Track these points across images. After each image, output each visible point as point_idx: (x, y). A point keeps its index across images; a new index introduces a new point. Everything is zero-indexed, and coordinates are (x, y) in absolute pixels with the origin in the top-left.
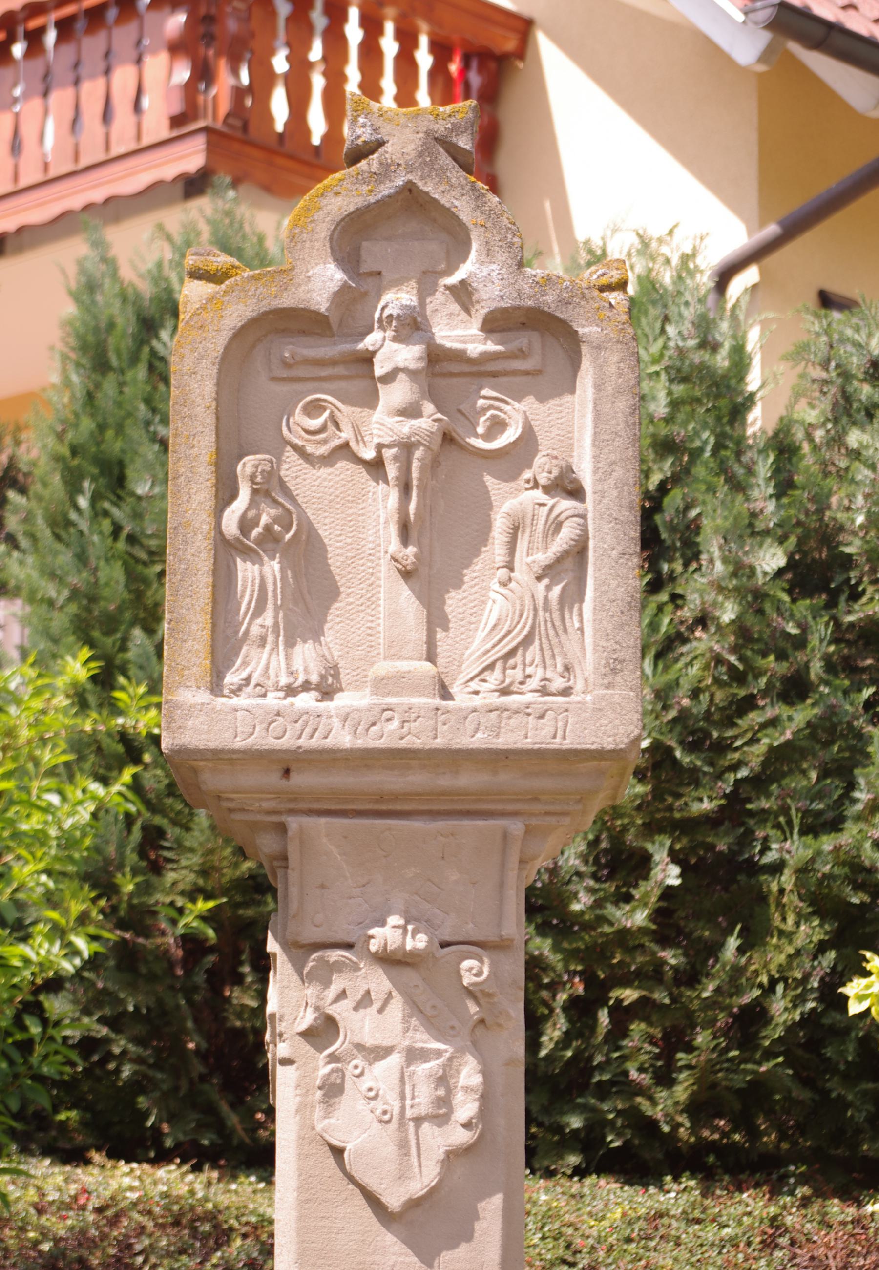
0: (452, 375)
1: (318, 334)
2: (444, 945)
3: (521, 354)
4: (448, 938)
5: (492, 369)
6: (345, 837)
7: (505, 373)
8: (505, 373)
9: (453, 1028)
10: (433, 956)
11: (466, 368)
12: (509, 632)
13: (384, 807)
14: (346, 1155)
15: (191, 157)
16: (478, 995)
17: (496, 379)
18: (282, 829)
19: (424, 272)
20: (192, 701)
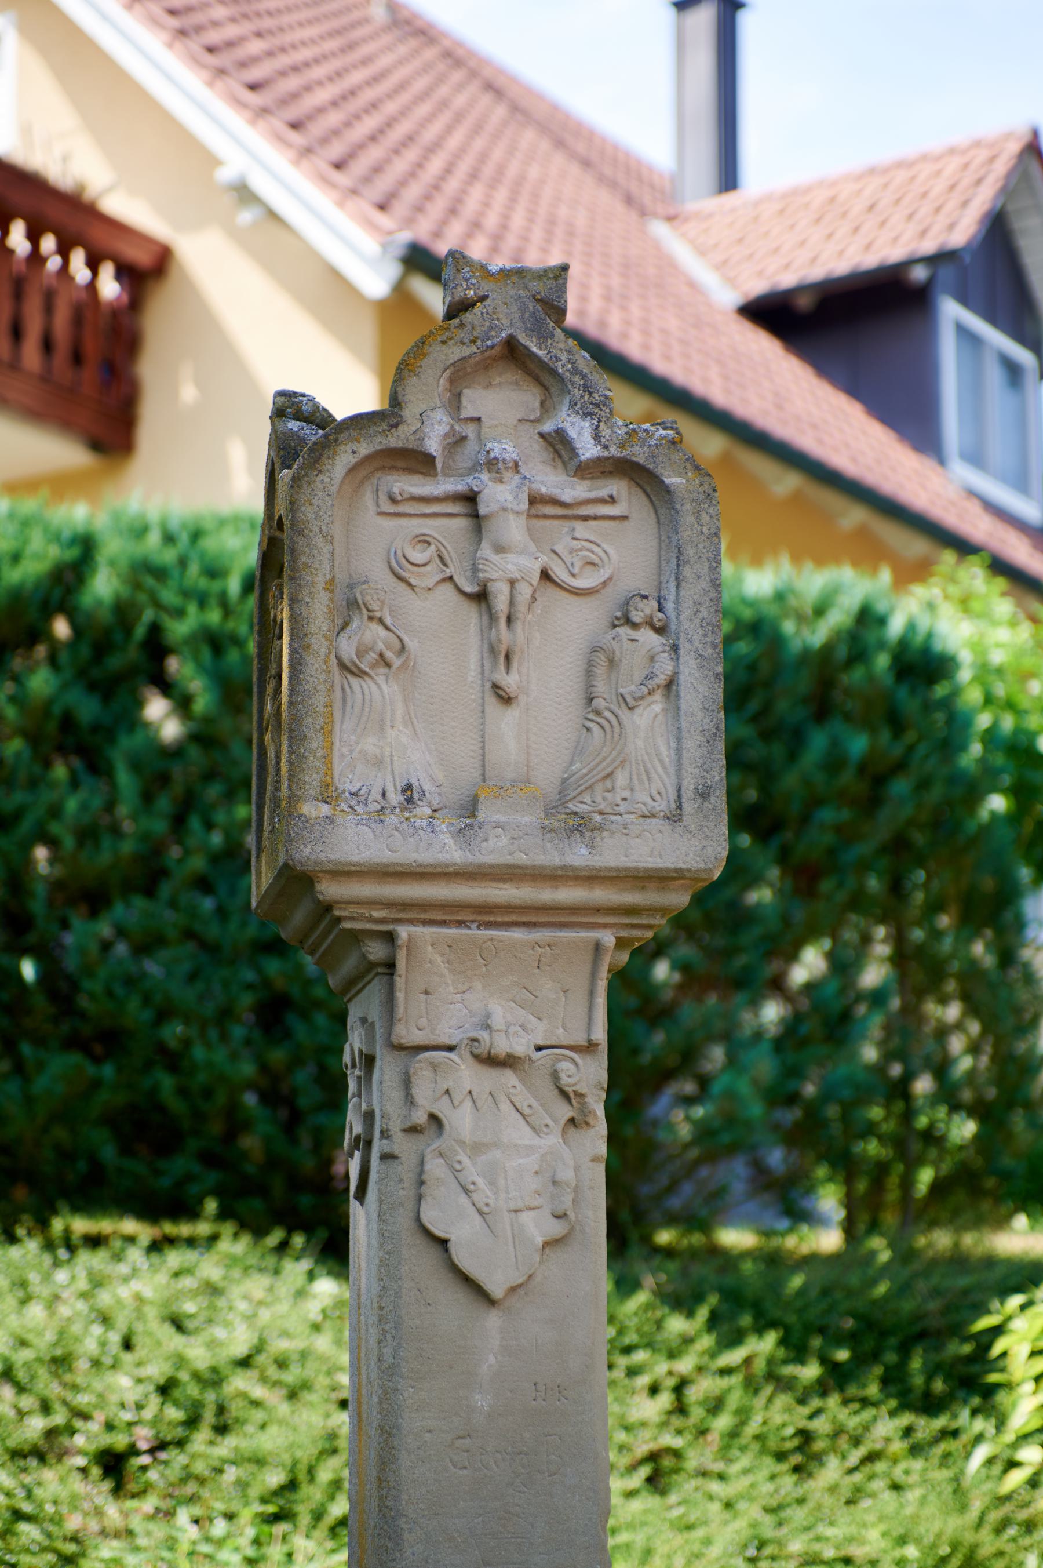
0: (546, 517)
1: (422, 473)
2: (539, 1048)
3: (612, 500)
4: (541, 1043)
5: (584, 513)
6: (450, 946)
7: (595, 518)
8: (595, 518)
9: (547, 1126)
10: (530, 1059)
11: (560, 511)
12: (605, 758)
13: (489, 915)
14: (450, 1245)
16: (572, 1095)
17: (586, 523)
18: (390, 937)
19: (520, 420)
20: (314, 814)
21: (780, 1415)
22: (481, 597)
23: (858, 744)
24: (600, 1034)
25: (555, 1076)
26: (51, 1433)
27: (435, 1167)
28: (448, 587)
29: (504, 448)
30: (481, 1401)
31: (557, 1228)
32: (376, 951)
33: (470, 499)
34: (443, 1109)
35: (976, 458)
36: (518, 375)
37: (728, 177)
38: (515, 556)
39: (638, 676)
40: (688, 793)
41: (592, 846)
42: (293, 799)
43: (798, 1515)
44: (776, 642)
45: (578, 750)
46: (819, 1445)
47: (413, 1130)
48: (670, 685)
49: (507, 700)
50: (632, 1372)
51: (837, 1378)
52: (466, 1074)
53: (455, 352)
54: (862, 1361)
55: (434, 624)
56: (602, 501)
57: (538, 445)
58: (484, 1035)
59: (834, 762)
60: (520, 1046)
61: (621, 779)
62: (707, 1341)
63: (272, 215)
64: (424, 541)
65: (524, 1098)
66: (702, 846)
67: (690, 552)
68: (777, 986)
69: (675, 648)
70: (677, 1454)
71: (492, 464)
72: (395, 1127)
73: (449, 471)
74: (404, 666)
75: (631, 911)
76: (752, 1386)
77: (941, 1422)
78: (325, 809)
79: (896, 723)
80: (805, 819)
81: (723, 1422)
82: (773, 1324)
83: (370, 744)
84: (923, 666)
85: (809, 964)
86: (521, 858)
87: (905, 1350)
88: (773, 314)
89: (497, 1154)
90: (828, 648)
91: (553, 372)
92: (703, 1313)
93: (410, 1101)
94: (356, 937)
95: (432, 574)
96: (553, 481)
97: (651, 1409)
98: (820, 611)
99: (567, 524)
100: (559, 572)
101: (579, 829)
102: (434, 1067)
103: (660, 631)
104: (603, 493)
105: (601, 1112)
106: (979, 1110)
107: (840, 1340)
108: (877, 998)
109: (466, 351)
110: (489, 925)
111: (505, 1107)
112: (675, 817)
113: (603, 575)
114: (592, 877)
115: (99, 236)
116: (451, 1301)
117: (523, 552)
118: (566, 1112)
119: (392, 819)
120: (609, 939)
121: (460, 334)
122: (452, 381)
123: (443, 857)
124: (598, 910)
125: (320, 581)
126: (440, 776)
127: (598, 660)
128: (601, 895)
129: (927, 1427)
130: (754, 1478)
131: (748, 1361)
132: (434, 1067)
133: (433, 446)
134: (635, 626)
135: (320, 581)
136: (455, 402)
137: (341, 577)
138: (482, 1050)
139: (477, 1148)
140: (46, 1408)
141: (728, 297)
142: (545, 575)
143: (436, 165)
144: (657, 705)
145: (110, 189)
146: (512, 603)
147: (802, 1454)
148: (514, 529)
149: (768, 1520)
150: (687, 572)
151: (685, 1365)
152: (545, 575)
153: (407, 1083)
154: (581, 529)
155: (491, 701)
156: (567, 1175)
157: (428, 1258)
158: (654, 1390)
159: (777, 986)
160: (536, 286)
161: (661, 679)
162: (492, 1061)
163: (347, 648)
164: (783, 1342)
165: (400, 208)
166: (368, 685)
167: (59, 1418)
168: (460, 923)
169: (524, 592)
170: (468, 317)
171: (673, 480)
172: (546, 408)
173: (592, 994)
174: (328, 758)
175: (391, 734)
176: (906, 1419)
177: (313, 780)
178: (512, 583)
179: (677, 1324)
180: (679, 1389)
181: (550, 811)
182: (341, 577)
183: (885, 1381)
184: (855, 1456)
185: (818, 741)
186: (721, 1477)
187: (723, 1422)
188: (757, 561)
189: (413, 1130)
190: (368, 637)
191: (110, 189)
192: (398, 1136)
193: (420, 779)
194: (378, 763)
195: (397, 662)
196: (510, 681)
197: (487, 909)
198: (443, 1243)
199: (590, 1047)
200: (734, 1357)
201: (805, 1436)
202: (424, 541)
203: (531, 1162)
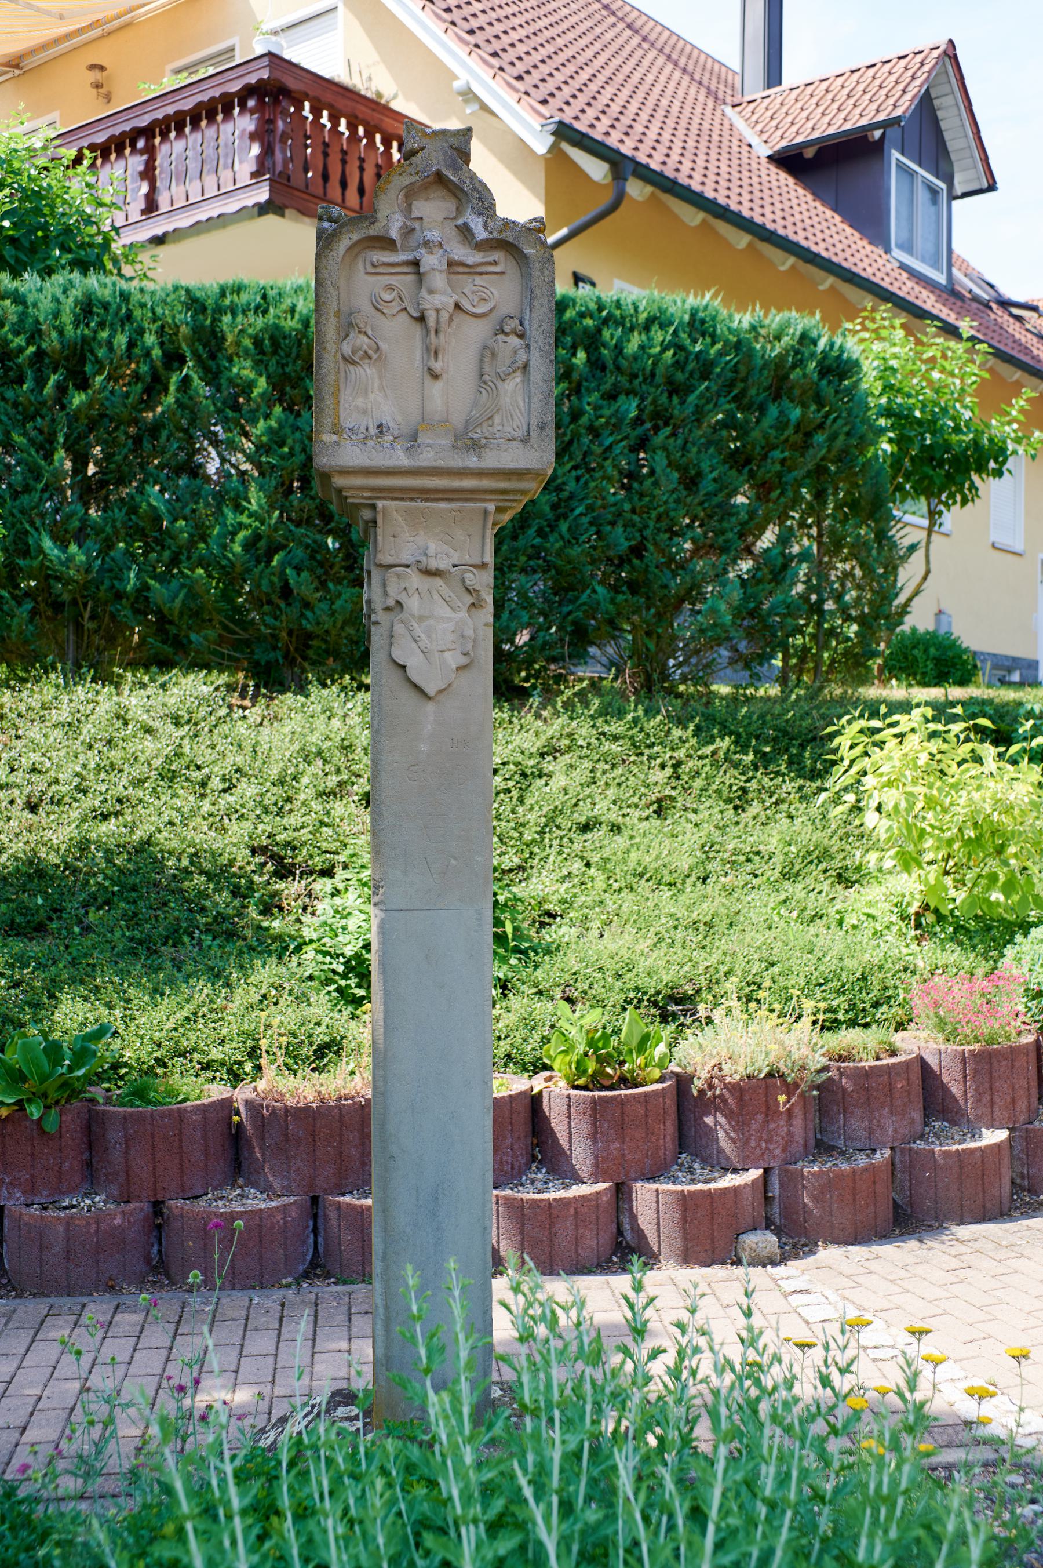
3: (495, 263)
15: (262, 194)
18: (373, 507)
21: (731, 778)
22: (422, 319)
23: (796, 413)
24: (489, 558)
25: (463, 581)
26: (340, 784)
27: (399, 628)
28: (404, 315)
29: (434, 234)
30: (424, 748)
31: (464, 660)
32: (367, 514)
33: (416, 263)
34: (403, 598)
35: (908, 247)
36: (445, 193)
37: (773, 75)
38: (440, 297)
39: (508, 362)
40: (533, 427)
41: (480, 456)
43: (734, 831)
44: (750, 353)
45: (475, 404)
46: (750, 796)
47: (388, 609)
48: (526, 366)
49: (436, 377)
50: (650, 758)
51: (764, 760)
52: (415, 580)
53: (407, 180)
54: (777, 752)
55: (396, 334)
56: (490, 264)
57: (454, 232)
58: (424, 559)
59: (782, 424)
60: (443, 564)
61: (497, 419)
62: (693, 741)
63: (485, 108)
64: (390, 288)
65: (446, 592)
66: (541, 457)
67: (537, 291)
68: (749, 551)
69: (528, 346)
70: (673, 799)
71: (426, 244)
73: (405, 249)
74: (379, 358)
75: (504, 492)
76: (716, 765)
78: (335, 437)
79: (819, 400)
80: (765, 457)
81: (698, 783)
82: (730, 734)
83: (360, 402)
84: (839, 369)
85: (768, 539)
86: (441, 463)
87: (802, 747)
88: (790, 161)
89: (432, 622)
90: (782, 357)
91: (462, 190)
92: (692, 727)
93: (386, 594)
94: (357, 506)
95: (395, 307)
96: (462, 253)
97: (660, 776)
98: (778, 338)
99: (469, 278)
100: (465, 304)
101: (472, 447)
102: (398, 576)
103: (521, 336)
104: (490, 259)
105: (490, 600)
106: (861, 620)
108: (804, 556)
109: (413, 179)
110: (427, 500)
111: (436, 597)
112: (526, 440)
114: (481, 473)
115: (389, 124)
116: (408, 697)
117: (444, 293)
118: (469, 600)
119: (370, 443)
120: (491, 507)
121: (410, 170)
122: (407, 197)
123: (398, 463)
124: (486, 491)
125: (332, 311)
126: (399, 419)
127: (487, 353)
128: (486, 483)
130: (712, 811)
131: (714, 753)
132: (398, 576)
133: (394, 234)
134: (506, 334)
135: (332, 311)
136: (408, 209)
137: (344, 309)
138: (423, 566)
139: (421, 619)
140: (338, 771)
141: (765, 151)
142: (457, 306)
143: (584, 76)
144: (518, 378)
145: (395, 97)
146: (438, 322)
147: (740, 801)
148: (439, 280)
149: (717, 833)
150: (536, 303)
151: (681, 754)
152: (457, 306)
153: (384, 585)
154: (478, 280)
155: (427, 377)
156: (469, 632)
157: (396, 675)
158: (663, 766)
159: (749, 551)
160: (452, 141)
161: (520, 364)
163: (347, 348)
164: (736, 743)
165: (556, 103)
166: (358, 369)
167: (345, 777)
168: (412, 499)
169: (445, 316)
170: (414, 159)
171: (528, 251)
172: (459, 211)
173: (484, 537)
174: (336, 410)
175: (372, 396)
177: (328, 421)
178: (438, 311)
179: (677, 732)
180: (678, 765)
181: (457, 438)
182: (344, 309)
183: (790, 763)
184: (769, 802)
185: (773, 411)
186: (695, 811)
187: (698, 783)
188: (742, 308)
189: (388, 609)
190: (358, 342)
191: (395, 97)
192: (380, 613)
193: (387, 420)
194: (365, 412)
195: (375, 356)
196: (437, 366)
197: (425, 491)
199: (483, 566)
200: (708, 750)
201: (744, 791)
202: (390, 288)
203: (450, 626)
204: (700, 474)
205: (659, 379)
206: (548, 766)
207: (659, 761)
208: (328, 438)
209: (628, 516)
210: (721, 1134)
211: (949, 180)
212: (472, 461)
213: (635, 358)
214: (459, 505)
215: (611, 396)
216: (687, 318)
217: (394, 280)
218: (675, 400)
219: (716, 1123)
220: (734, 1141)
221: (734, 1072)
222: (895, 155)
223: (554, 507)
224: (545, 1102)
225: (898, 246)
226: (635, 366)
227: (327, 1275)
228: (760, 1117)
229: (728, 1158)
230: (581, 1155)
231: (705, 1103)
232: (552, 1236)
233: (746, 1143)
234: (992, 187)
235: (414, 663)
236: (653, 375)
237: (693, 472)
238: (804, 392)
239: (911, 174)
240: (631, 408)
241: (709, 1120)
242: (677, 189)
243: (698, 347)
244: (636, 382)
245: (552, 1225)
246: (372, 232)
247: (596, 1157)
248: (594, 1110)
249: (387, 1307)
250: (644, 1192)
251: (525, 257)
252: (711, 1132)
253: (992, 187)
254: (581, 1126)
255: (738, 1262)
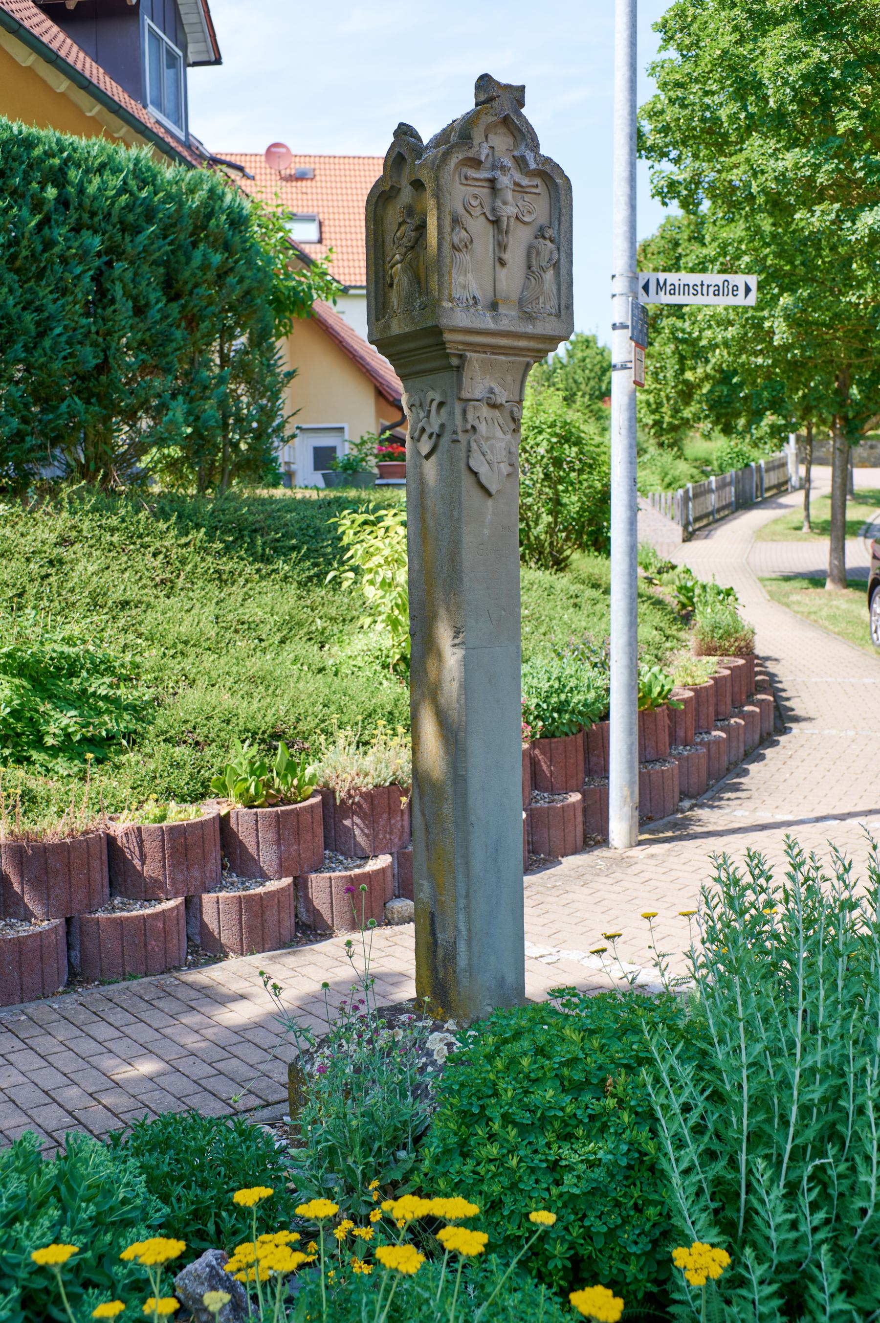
13: (495, 349)
27: (474, 446)
30: (486, 532)
33: (492, 181)
34: (476, 423)
35: (159, 106)
42: (440, 300)
45: (525, 288)
47: (466, 431)
50: (146, 546)
52: (485, 411)
64: (476, 197)
72: (459, 430)
77: (271, 567)
79: (227, 247)
83: (461, 279)
86: (512, 329)
91: (520, 131)
107: (229, 532)
113: (534, 216)
119: (472, 310)
124: (529, 350)
127: (531, 251)
129: (265, 569)
134: (544, 238)
139: (487, 439)
148: (509, 195)
153: (464, 412)
154: (527, 197)
155: (497, 264)
162: (494, 406)
172: (516, 146)
176: (257, 566)
179: (162, 526)
189: (466, 431)
198: (475, 474)
202: (476, 197)
203: (503, 445)
204: (147, 305)
205: (114, 219)
206: (67, 554)
207: (152, 549)
208: (446, 304)
209: (94, 336)
210: (357, 832)
211: (184, 48)
212: (530, 329)
213: (95, 198)
214: (511, 358)
215: (77, 229)
216: (131, 166)
217: (477, 191)
218: (128, 239)
219: (353, 823)
220: (367, 836)
221: (367, 784)
222: (148, 21)
223: (38, 324)
224: (233, 821)
225: (152, 103)
226: (96, 204)
227: (88, 980)
228: (385, 816)
229: (363, 849)
230: (267, 858)
231: (345, 810)
232: (264, 921)
233: (376, 837)
234: (218, 61)
235: (483, 470)
236: (110, 214)
237: (143, 302)
238: (216, 240)
239: (159, 39)
240: (96, 243)
241: (347, 823)
242: (22, 31)
243: (144, 194)
244: (96, 219)
245: (263, 913)
246: (470, 155)
247: (280, 859)
248: (278, 822)
249: (469, 931)
250: (318, 882)
251: (556, 185)
252: (349, 831)
253: (218, 61)
254: (267, 836)
255: (389, 923)
